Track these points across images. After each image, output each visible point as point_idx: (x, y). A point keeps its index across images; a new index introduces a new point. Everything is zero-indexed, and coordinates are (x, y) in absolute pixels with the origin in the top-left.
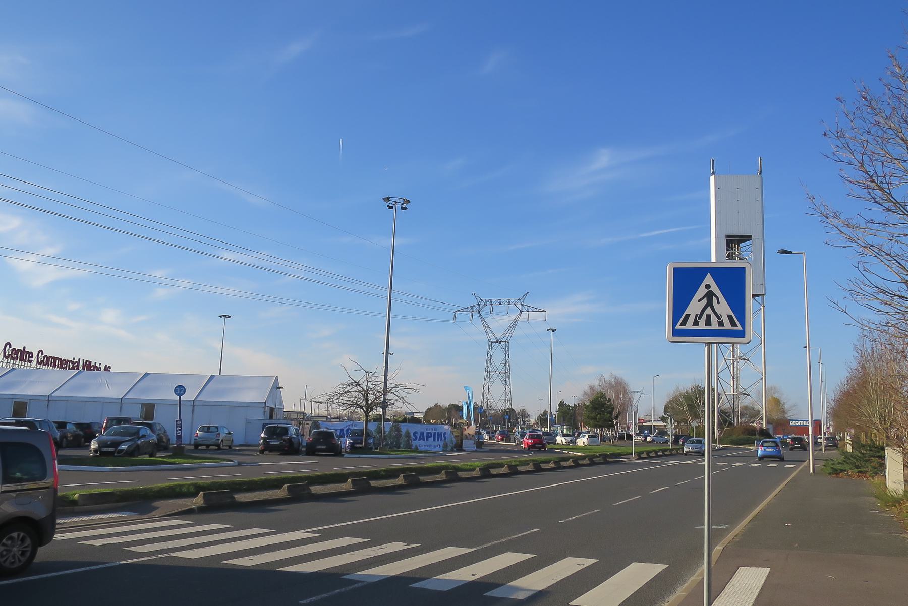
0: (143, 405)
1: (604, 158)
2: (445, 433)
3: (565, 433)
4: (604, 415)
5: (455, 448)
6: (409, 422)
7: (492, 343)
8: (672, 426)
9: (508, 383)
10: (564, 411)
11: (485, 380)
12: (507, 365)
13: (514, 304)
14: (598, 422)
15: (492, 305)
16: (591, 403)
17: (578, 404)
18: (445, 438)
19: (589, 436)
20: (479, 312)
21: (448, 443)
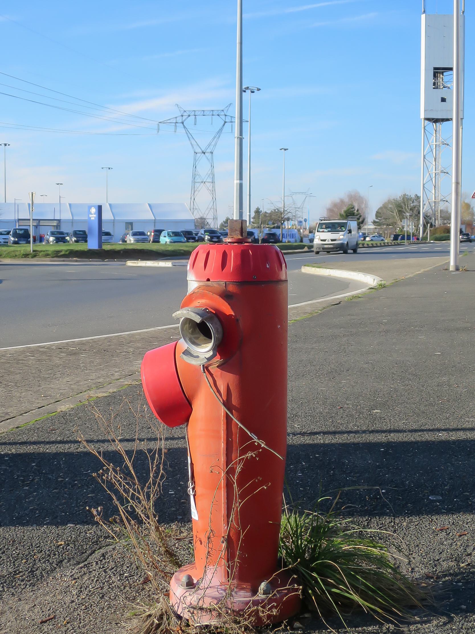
0: (126, 223)
6: (276, 228)
13: (218, 115)
20: (183, 123)
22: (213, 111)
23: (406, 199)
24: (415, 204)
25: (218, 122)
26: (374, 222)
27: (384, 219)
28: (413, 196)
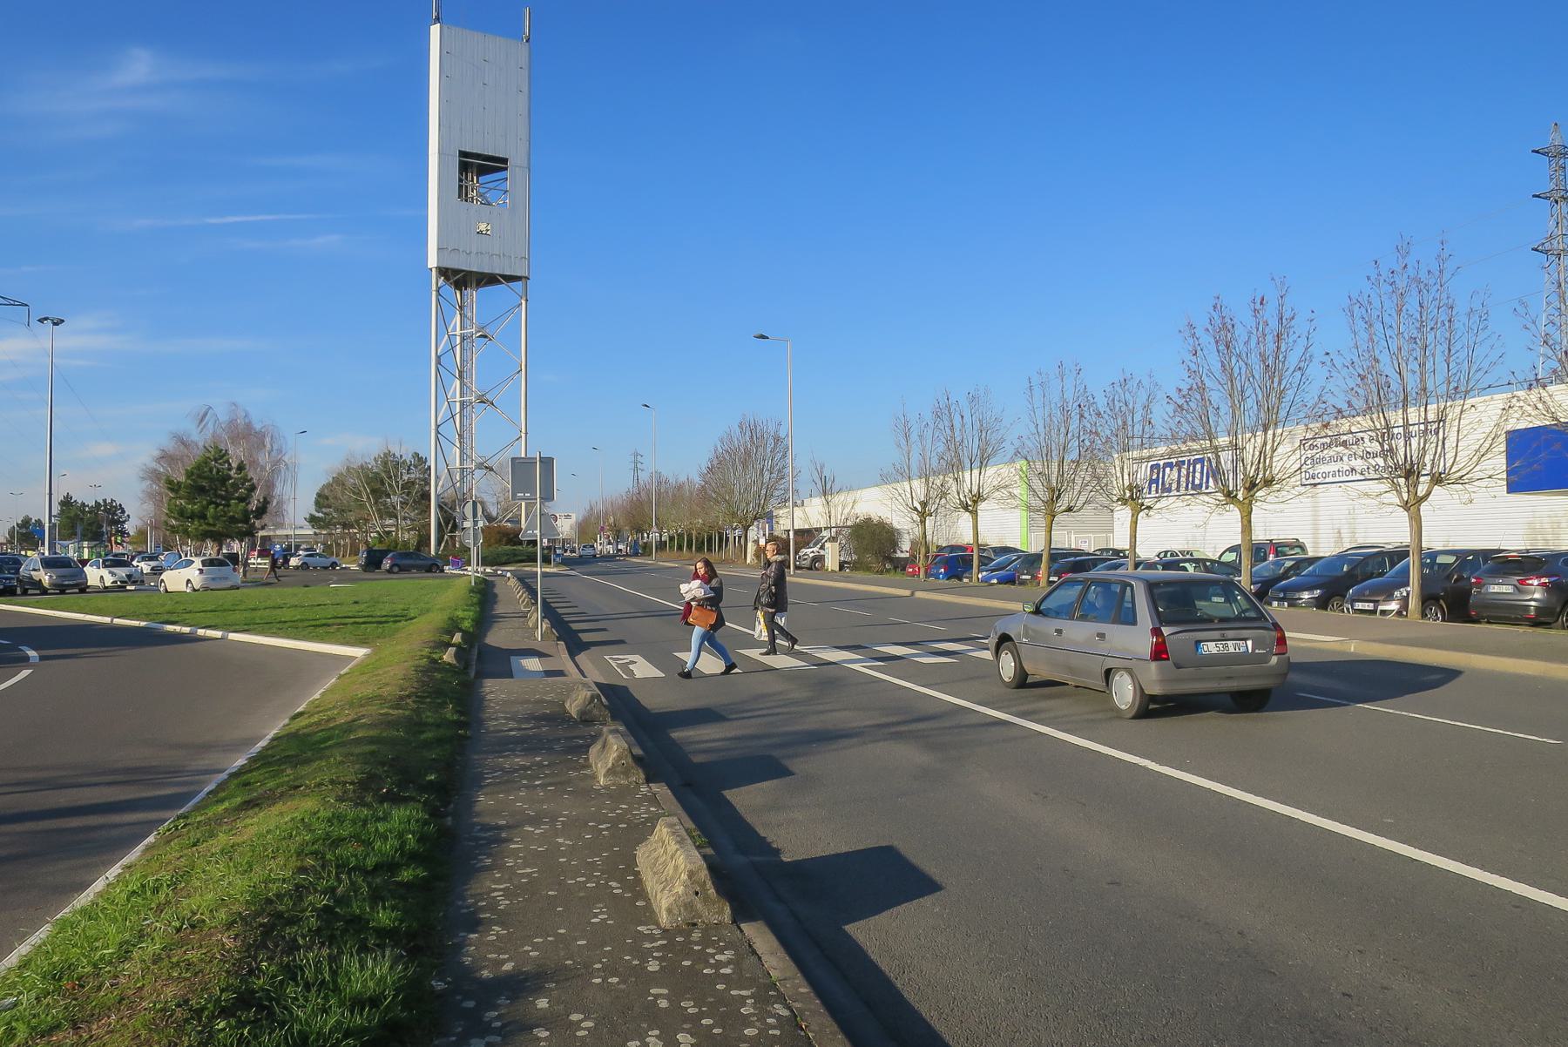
4: (228, 505)
8: (475, 523)
10: (72, 514)
14: (209, 524)
16: (189, 474)
17: (105, 501)
19: (204, 563)
23: (390, 464)
24: (413, 476)
26: (313, 520)
28: (408, 458)
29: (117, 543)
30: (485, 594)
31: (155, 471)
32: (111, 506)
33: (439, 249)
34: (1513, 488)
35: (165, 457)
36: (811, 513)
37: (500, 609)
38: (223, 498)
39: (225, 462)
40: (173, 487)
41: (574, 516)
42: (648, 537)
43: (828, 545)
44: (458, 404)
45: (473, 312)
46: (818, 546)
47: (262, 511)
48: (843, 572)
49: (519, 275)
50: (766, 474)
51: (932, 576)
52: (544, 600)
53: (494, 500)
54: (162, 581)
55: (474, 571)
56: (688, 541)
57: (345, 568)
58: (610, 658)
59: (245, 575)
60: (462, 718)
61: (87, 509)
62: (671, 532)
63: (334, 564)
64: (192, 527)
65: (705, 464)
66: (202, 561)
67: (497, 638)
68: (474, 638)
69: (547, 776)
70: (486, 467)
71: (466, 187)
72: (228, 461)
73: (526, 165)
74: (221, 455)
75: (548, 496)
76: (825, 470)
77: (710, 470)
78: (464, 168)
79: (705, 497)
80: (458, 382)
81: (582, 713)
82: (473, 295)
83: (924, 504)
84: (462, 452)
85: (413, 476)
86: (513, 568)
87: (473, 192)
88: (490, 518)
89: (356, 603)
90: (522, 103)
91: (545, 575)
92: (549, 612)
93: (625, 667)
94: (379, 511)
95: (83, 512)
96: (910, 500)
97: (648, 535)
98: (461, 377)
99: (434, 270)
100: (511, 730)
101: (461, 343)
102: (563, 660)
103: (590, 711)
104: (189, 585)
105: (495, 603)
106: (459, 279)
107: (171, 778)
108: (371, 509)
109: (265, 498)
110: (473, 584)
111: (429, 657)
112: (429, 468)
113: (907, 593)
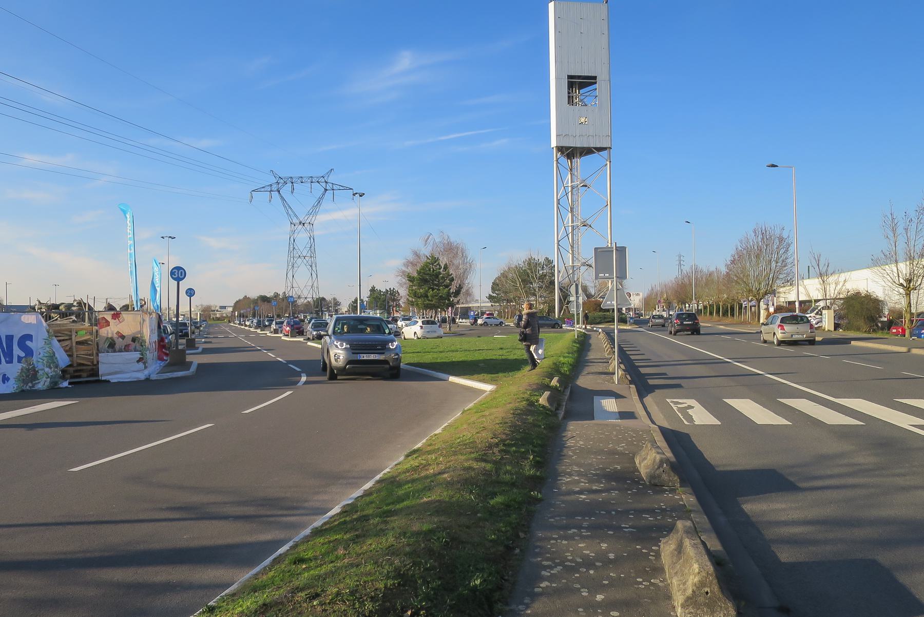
1: (405, 60)
2: (29, 337)
3: (196, 340)
4: (438, 290)
5: (63, 378)
7: (295, 225)
8: (578, 298)
9: (314, 268)
10: (375, 296)
11: (288, 266)
12: (312, 248)
13: (318, 182)
14: (429, 300)
15: (292, 183)
16: (419, 273)
17: (390, 289)
18: (29, 352)
21: (39, 366)
22: (312, 177)
23: (532, 264)
24: (545, 271)
25: (318, 189)
26: (490, 298)
27: (503, 292)
28: (542, 260)
29: (396, 311)
30: (583, 343)
31: (404, 272)
32: (394, 292)
33: (557, 136)
34: (13, 336)
35: (409, 263)
36: (810, 289)
37: (591, 355)
38: (436, 285)
39: (437, 265)
40: (411, 279)
41: (641, 294)
42: (689, 307)
43: (824, 312)
44: (570, 228)
45: (579, 173)
46: (815, 312)
47: (457, 293)
48: (837, 332)
49: (605, 146)
50: (774, 265)
51: (914, 335)
52: (619, 346)
53: (592, 285)
54: (403, 332)
55: (579, 328)
56: (716, 309)
57: (507, 325)
58: (672, 402)
59: (450, 329)
60: (538, 474)
61: (382, 293)
62: (705, 303)
63: (501, 323)
64: (420, 301)
65: (729, 258)
66: (422, 322)
67: (584, 381)
68: (568, 379)
69: (613, 584)
70: (588, 265)
71: (572, 97)
72: (439, 264)
73: (608, 79)
74: (435, 260)
75: (622, 276)
76: (821, 259)
77: (733, 262)
78: (571, 85)
79: (729, 280)
80: (570, 214)
81: (652, 477)
82: (578, 162)
83: (909, 281)
84: (573, 257)
85: (545, 271)
86: (603, 326)
87: (576, 99)
88: (589, 296)
89: (501, 349)
90: (604, 41)
91: (620, 331)
92: (624, 357)
93: (684, 410)
94: (526, 292)
95: (380, 295)
96: (897, 278)
97: (689, 305)
98: (572, 211)
99: (555, 148)
100: (581, 492)
101: (571, 191)
102: (633, 402)
103: (659, 476)
104: (416, 335)
105: (589, 350)
106: (570, 153)
107: (290, 515)
108: (522, 292)
109: (460, 285)
110: (576, 337)
111: (527, 400)
112: (554, 266)
113: (904, 349)
